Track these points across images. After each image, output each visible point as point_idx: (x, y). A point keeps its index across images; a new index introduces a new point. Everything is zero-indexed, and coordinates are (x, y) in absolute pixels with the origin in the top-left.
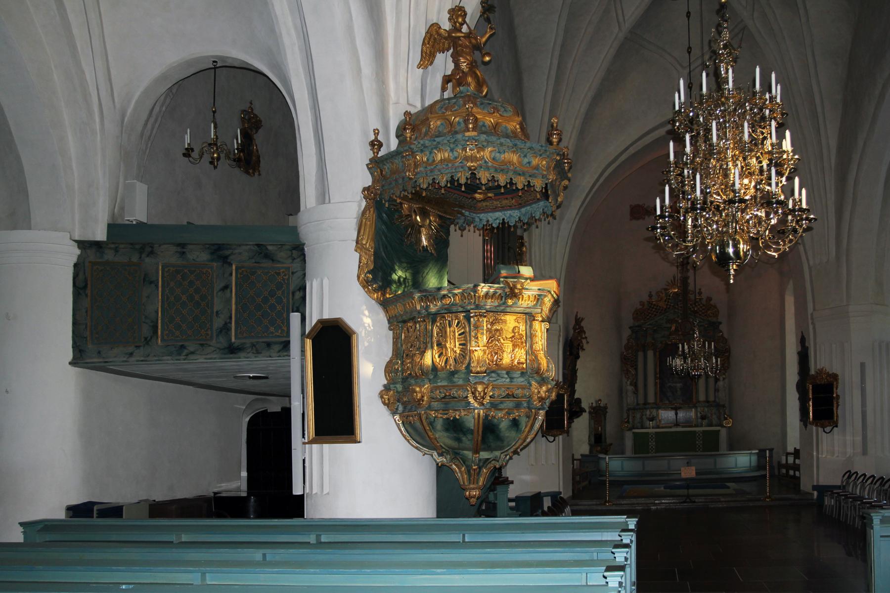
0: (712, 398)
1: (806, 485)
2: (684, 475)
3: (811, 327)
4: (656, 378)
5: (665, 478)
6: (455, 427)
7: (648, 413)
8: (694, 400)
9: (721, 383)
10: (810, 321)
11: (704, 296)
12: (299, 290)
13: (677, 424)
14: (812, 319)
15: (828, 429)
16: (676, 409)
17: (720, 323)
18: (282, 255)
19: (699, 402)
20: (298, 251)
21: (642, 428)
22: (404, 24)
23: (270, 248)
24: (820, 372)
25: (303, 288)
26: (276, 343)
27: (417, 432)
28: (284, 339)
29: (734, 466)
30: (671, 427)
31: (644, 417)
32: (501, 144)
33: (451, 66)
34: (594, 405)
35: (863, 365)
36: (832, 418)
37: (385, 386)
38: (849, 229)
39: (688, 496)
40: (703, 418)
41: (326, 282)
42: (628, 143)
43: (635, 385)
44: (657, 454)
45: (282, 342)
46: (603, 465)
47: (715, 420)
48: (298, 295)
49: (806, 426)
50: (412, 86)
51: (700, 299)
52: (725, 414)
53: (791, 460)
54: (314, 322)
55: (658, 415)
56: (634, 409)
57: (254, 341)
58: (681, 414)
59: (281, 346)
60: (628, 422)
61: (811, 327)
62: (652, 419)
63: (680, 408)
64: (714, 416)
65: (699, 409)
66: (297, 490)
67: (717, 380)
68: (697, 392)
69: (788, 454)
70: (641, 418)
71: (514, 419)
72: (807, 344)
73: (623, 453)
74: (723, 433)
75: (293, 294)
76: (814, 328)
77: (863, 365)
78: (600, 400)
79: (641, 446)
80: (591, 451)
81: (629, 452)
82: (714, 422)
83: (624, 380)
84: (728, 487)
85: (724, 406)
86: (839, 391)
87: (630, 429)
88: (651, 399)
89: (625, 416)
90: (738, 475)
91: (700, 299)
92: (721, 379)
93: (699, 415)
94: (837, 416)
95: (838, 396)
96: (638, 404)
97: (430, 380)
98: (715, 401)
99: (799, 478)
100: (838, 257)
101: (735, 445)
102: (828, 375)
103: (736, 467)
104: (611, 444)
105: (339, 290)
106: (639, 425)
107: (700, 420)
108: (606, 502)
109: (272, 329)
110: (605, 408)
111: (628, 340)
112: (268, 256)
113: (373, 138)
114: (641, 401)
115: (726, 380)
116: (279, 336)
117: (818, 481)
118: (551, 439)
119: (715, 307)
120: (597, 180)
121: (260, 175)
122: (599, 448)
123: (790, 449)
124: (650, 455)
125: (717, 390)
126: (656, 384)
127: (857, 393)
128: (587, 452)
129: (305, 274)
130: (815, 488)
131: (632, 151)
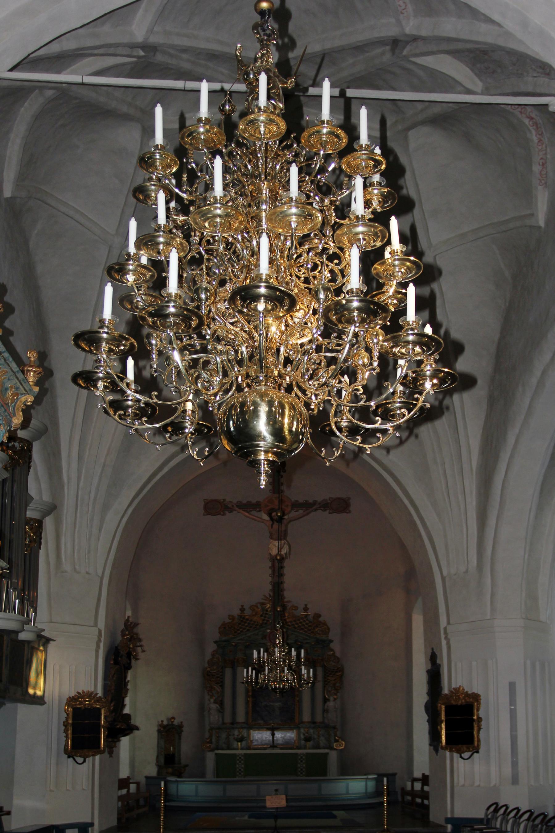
0: (319, 719)
3: (444, 642)
4: (247, 696)
7: (236, 732)
9: (331, 704)
10: (443, 636)
11: (311, 613)
16: (273, 730)
17: (331, 641)
19: (303, 722)
21: (229, 748)
24: (456, 692)
30: (265, 749)
31: (231, 738)
34: (165, 723)
35: (512, 686)
40: (307, 739)
43: (221, 703)
47: (323, 741)
52: (336, 735)
55: (249, 735)
56: (219, 728)
58: (279, 735)
60: (211, 742)
61: (444, 642)
62: (241, 740)
63: (278, 729)
65: (302, 730)
67: (325, 700)
69: (414, 780)
73: (203, 775)
74: (333, 756)
76: (449, 648)
77: (512, 686)
78: (174, 718)
80: (159, 773)
82: (322, 744)
83: (207, 697)
84: (335, 817)
85: (334, 728)
87: (212, 750)
88: (241, 717)
89: (207, 735)
91: (306, 616)
93: (302, 737)
94: (479, 741)
95: (480, 719)
96: (224, 723)
99: (427, 807)
101: (347, 769)
102: (467, 695)
103: (348, 793)
104: (187, 766)
107: (303, 742)
110: (181, 726)
111: (213, 655)
114: (228, 719)
118: (80, 760)
119: (325, 624)
122: (170, 770)
123: (417, 774)
124: (237, 779)
126: (247, 703)
127: (505, 717)
130: (448, 821)
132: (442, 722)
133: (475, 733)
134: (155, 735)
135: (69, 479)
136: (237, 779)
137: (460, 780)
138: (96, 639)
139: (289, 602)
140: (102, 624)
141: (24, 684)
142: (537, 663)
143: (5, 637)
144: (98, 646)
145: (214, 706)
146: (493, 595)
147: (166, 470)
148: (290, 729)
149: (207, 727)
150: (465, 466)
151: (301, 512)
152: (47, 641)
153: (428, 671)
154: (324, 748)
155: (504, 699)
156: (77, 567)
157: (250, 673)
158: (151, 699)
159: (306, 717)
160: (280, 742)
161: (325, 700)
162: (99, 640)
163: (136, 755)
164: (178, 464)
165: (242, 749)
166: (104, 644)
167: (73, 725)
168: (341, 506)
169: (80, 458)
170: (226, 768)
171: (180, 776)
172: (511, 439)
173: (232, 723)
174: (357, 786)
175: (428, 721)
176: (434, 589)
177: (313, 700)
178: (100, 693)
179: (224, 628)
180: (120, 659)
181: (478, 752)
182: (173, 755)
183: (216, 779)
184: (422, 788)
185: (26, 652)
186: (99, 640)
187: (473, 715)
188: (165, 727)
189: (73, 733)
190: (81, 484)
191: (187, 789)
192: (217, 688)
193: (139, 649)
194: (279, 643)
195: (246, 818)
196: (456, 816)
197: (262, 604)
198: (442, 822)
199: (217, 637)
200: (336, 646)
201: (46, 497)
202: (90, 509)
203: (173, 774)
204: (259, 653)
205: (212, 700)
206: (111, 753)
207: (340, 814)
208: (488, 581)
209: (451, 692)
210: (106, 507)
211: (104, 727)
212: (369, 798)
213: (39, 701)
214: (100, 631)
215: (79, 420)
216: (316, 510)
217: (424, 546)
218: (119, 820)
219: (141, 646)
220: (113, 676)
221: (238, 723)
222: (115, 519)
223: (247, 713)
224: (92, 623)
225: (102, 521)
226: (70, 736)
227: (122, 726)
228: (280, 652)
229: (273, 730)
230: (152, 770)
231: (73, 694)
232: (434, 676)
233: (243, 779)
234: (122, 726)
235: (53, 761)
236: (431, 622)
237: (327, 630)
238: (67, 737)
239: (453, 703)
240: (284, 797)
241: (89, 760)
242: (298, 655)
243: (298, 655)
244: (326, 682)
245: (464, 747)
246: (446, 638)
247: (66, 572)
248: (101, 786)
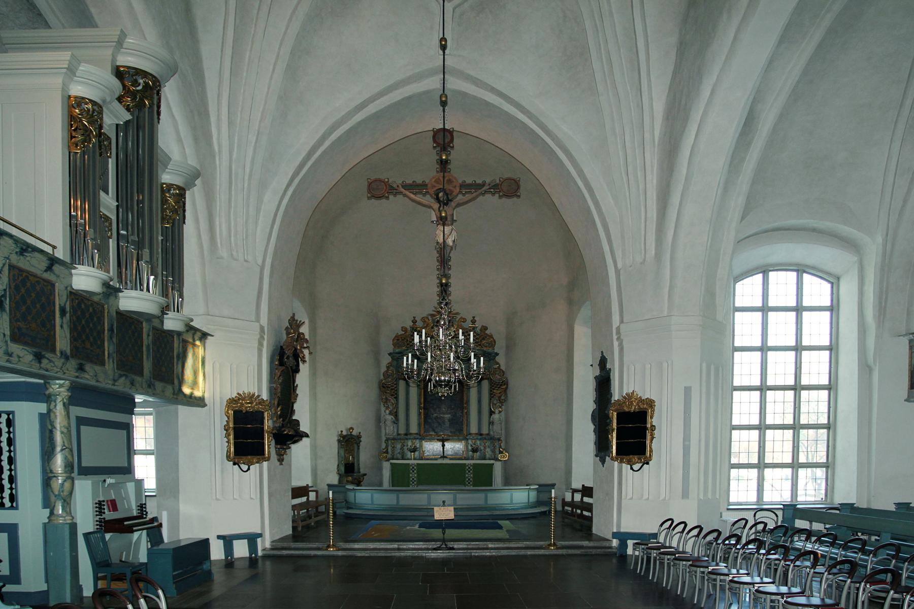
1: (598, 528)
2: (437, 517)
3: (616, 344)
4: (420, 408)
5: (425, 513)
7: (410, 443)
8: (465, 432)
9: (496, 417)
10: (615, 337)
13: (443, 457)
14: (618, 332)
15: (636, 467)
16: (443, 441)
17: (497, 354)
19: (470, 434)
21: (403, 459)
24: (629, 397)
29: (509, 502)
30: (436, 459)
31: (405, 448)
34: (344, 433)
35: (688, 391)
36: (644, 453)
39: (444, 541)
40: (475, 450)
42: (366, 96)
43: (396, 415)
44: (420, 487)
46: (351, 495)
47: (488, 453)
49: (603, 461)
52: (500, 447)
53: (577, 497)
55: (421, 446)
56: (394, 439)
58: (448, 445)
60: (387, 452)
61: (616, 344)
62: (414, 450)
63: (447, 440)
64: (488, 449)
65: (470, 441)
67: (491, 413)
68: (468, 425)
69: (575, 491)
70: (402, 448)
72: (608, 366)
73: (381, 484)
74: (498, 468)
76: (621, 349)
77: (688, 391)
79: (401, 478)
80: (340, 481)
81: (386, 484)
82: (488, 456)
83: (383, 409)
84: (500, 527)
85: (499, 439)
86: (654, 420)
87: (388, 460)
88: (414, 429)
89: (384, 446)
90: (513, 512)
92: (497, 411)
93: (470, 448)
94: (651, 451)
95: (653, 428)
96: (399, 434)
98: (488, 434)
99: (590, 519)
100: (658, 256)
101: (508, 481)
102: (641, 400)
103: (512, 503)
104: (365, 475)
106: (399, 456)
107: (471, 453)
108: (329, 546)
111: (388, 367)
114: (402, 431)
115: (503, 413)
117: (619, 525)
118: (245, 467)
119: (491, 336)
123: (576, 485)
124: (411, 488)
125: (491, 423)
126: (420, 414)
130: (615, 535)
131: (371, 109)
132: (613, 430)
133: (648, 442)
134: (336, 444)
136: (411, 488)
138: (258, 336)
139: (457, 314)
140: (264, 321)
141: (176, 382)
142: (712, 367)
143: (144, 324)
144: (261, 344)
145: (390, 418)
147: (327, 143)
148: (459, 440)
149: (384, 438)
150: (647, 136)
152: (204, 336)
153: (596, 378)
154: (490, 459)
155: (679, 407)
156: (235, 253)
157: (410, 361)
158: (327, 406)
160: (450, 453)
162: (262, 337)
163: (309, 462)
164: (339, 138)
165: (415, 459)
166: (268, 341)
167: (234, 428)
168: (509, 188)
169: (231, 123)
170: (401, 478)
171: (359, 484)
172: (706, 92)
173: (406, 435)
174: (519, 497)
175: (594, 431)
176: (608, 285)
177: (480, 412)
178: (265, 396)
180: (286, 361)
181: (648, 463)
182: (353, 464)
183: (391, 488)
184: (582, 499)
185: (176, 345)
186: (262, 337)
187: (645, 422)
188: (344, 437)
189: (235, 438)
190: (234, 156)
191: (365, 498)
192: (393, 401)
194: (445, 324)
195: (417, 527)
196: (622, 530)
197: (432, 315)
198: (609, 537)
199: (391, 349)
201: (192, 161)
202: (246, 185)
203: (352, 483)
204: (421, 336)
205: (388, 412)
206: (281, 460)
207: (505, 523)
209: (624, 397)
211: (268, 432)
212: (532, 507)
213: (199, 402)
214: (262, 328)
216: (483, 194)
217: (598, 235)
218: (294, 528)
219: (308, 347)
220: (279, 378)
221: (411, 434)
222: (273, 199)
223: (419, 425)
224: (253, 318)
225: (260, 201)
226: (232, 441)
227: (289, 434)
228: (445, 335)
229: (443, 441)
230: (334, 479)
231: (234, 395)
232: (603, 384)
233: (415, 488)
234: (289, 434)
235: (218, 468)
236: (601, 326)
237: (493, 344)
238: (228, 442)
239: (626, 409)
240: (452, 508)
241: (255, 468)
242: (467, 339)
243: (467, 339)
244: (491, 395)
246: (618, 339)
247: (222, 258)
248: (270, 495)
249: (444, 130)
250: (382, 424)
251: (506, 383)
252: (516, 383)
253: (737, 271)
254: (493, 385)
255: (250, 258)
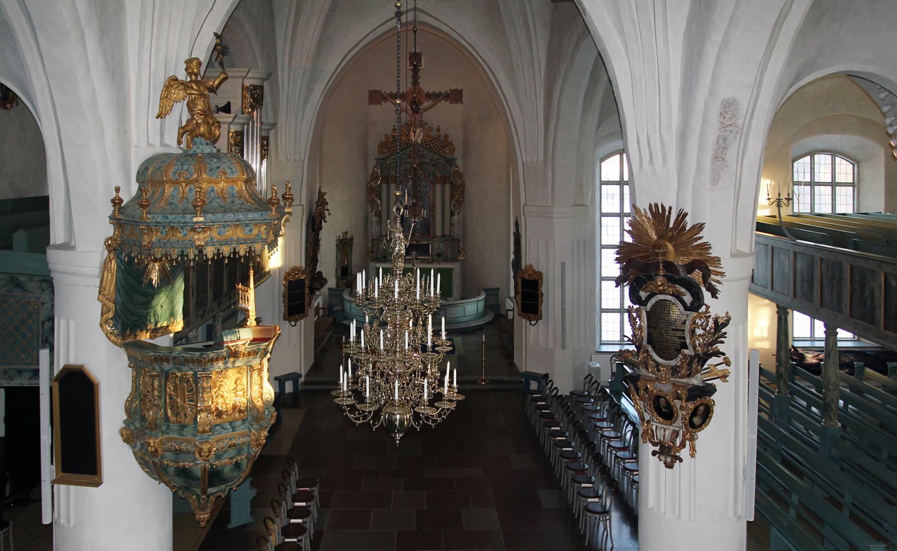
0: (447, 233)
3: (523, 218)
6: (184, 473)
9: (455, 218)
11: (442, 133)
12: (48, 320)
15: (533, 323)
18: (32, 286)
20: (47, 283)
22: (145, 73)
23: (21, 278)
25: (52, 319)
26: (27, 371)
27: (153, 465)
28: (34, 367)
32: (216, 287)
33: (186, 116)
35: (563, 265)
36: (537, 313)
37: (125, 422)
38: (554, 143)
41: (72, 323)
45: (33, 370)
48: (47, 325)
50: (153, 133)
51: (439, 136)
52: (459, 247)
54: (61, 367)
57: (7, 367)
59: (31, 374)
66: (46, 520)
67: (452, 214)
68: (434, 228)
71: (237, 463)
75: (43, 323)
77: (563, 265)
78: (347, 232)
80: (337, 284)
85: (458, 240)
89: (370, 245)
91: (439, 136)
95: (542, 294)
97: (162, 432)
98: (450, 236)
102: (535, 272)
105: (83, 338)
109: (23, 356)
110: (352, 239)
112: (19, 285)
113: (114, 195)
116: (30, 364)
118: (293, 323)
120: (340, 64)
121: (17, 105)
122: (345, 282)
125: (452, 225)
127: (558, 289)
128: (334, 286)
129: (53, 306)
131: (372, 37)
134: (334, 249)
135: (283, 84)
137: (531, 340)
145: (375, 219)
146: (553, 186)
147: (344, 63)
151: (431, 102)
159: (438, 232)
161: (452, 214)
177: (443, 214)
179: (382, 146)
187: (537, 289)
193: (326, 213)
200: (459, 163)
208: (550, 173)
210: (306, 101)
215: (289, 39)
245: (532, 316)
249: (415, 53)
250: (369, 225)
251: (463, 186)
252: (472, 187)
253: (602, 156)
254: (454, 188)
255: (297, 158)
